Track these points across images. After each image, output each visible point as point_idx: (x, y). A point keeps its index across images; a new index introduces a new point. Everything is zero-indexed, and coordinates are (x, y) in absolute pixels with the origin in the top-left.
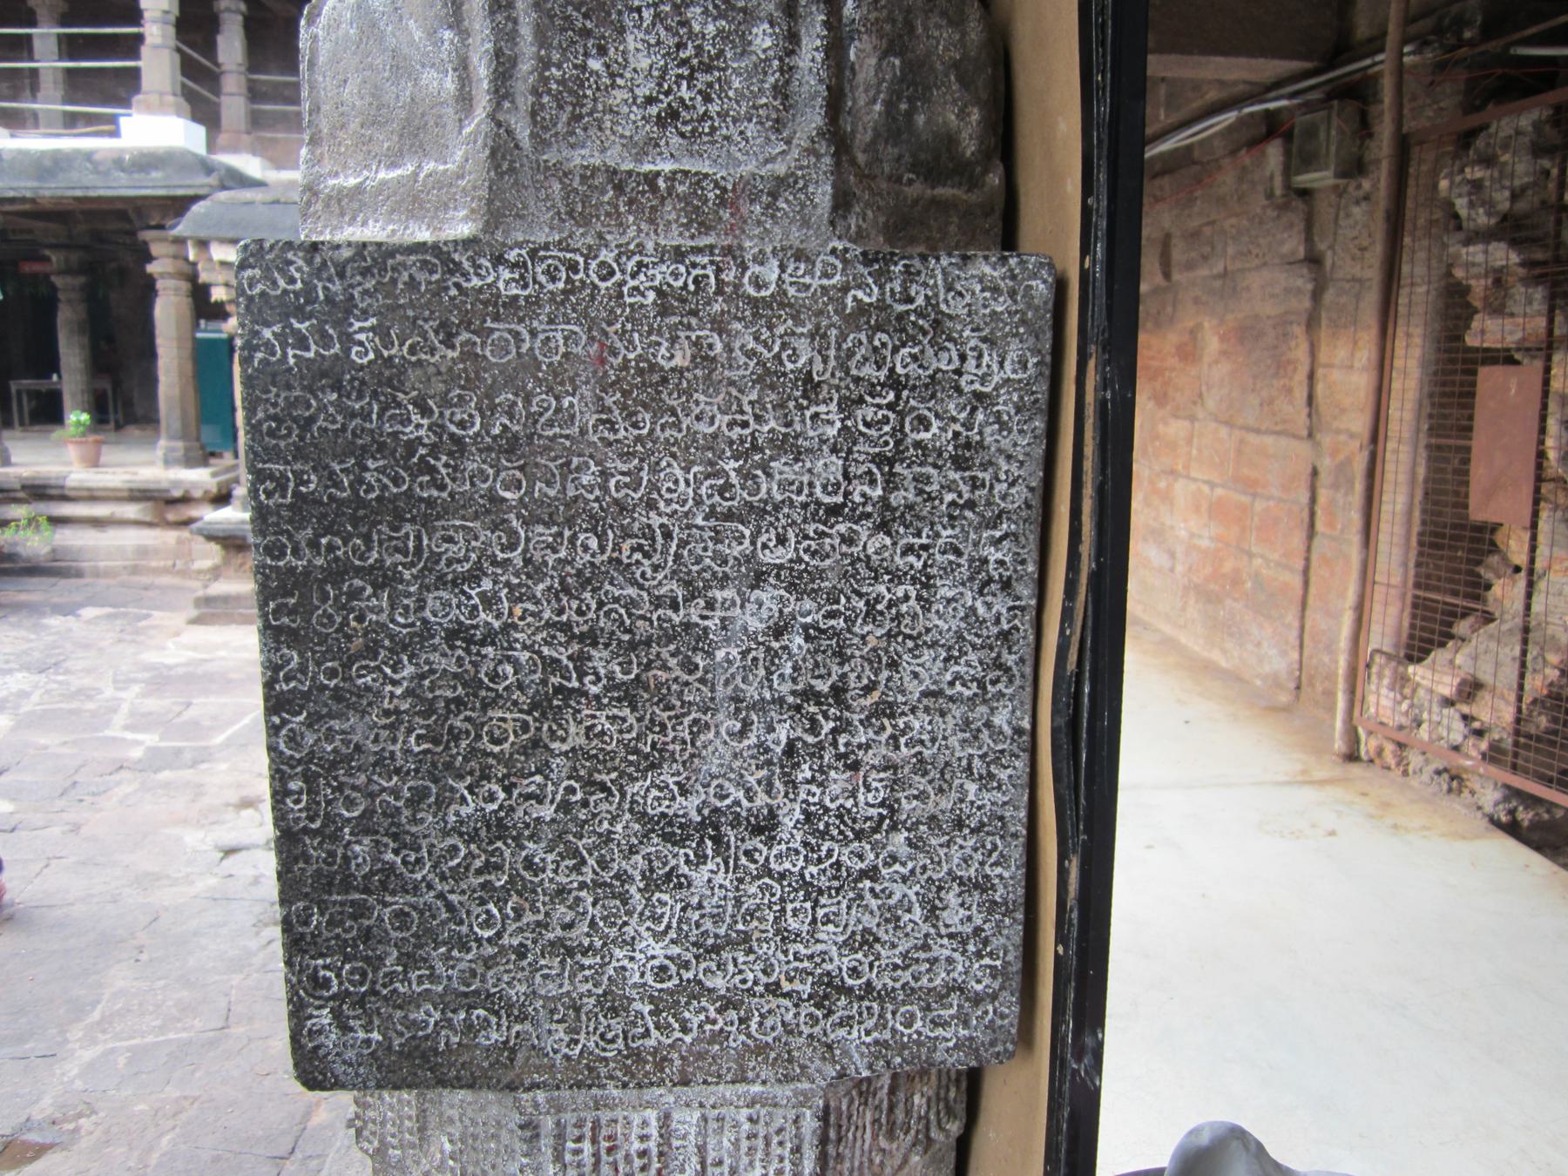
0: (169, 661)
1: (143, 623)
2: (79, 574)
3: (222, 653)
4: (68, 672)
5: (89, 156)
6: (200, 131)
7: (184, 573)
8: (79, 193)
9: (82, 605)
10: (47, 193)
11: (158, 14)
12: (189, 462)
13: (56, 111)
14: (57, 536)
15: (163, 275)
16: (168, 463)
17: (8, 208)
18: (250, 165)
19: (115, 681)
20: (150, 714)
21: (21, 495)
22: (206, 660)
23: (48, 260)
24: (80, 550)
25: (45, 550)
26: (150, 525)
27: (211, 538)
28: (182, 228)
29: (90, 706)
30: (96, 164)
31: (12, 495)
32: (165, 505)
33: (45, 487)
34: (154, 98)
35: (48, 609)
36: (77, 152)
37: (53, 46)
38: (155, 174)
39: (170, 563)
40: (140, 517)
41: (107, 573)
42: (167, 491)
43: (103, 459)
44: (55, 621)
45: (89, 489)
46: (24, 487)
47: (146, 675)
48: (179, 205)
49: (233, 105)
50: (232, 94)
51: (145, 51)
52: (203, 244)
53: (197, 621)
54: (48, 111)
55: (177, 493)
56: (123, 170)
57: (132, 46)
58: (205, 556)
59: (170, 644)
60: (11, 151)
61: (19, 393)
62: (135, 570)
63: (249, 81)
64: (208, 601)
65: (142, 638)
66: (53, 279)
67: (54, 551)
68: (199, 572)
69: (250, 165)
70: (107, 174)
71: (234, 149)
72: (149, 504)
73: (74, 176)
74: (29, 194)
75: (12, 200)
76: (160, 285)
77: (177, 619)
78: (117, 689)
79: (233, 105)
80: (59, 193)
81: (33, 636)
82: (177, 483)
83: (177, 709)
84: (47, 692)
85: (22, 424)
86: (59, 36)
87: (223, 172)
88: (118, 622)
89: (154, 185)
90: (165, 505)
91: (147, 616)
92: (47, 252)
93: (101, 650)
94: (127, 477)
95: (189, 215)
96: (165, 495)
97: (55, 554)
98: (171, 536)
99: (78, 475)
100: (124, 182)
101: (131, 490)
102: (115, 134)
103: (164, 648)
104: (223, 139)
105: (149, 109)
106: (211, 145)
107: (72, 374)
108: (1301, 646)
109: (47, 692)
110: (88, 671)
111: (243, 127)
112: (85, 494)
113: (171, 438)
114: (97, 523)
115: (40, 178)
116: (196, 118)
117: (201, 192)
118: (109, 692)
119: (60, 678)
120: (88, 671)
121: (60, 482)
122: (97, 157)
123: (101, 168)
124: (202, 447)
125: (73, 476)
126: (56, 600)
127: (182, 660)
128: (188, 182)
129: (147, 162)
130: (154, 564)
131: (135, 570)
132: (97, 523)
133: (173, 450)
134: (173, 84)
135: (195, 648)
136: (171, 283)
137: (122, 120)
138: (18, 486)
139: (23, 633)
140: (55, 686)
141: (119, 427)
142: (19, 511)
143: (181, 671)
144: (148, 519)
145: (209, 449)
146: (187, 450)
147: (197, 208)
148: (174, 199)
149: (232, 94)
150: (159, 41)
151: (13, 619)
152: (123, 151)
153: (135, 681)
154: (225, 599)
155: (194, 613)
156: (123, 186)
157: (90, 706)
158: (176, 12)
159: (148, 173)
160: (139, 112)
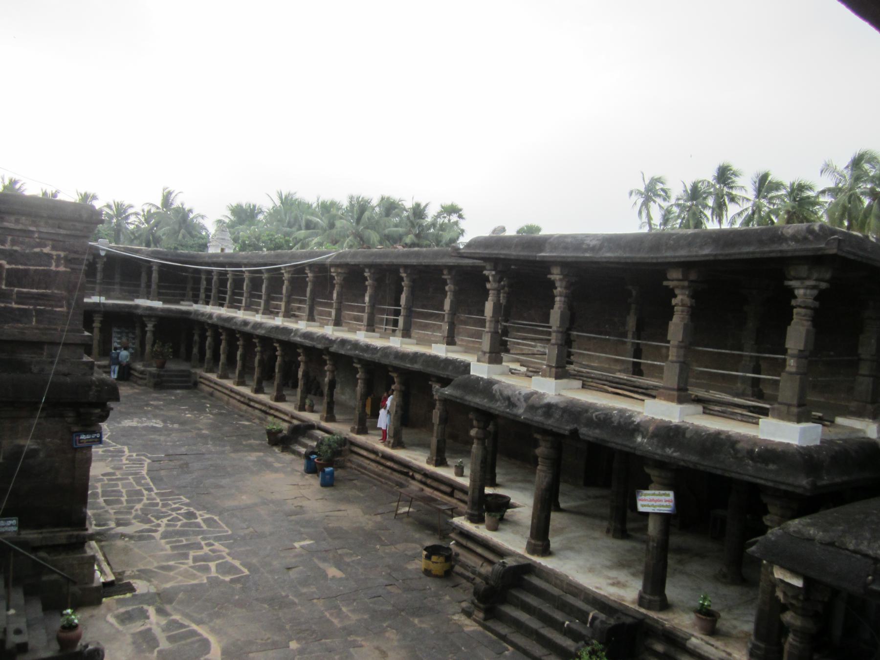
30: (737, 451)
50: (864, 376)
56: (752, 459)
149: (864, 376)
159: (767, 465)
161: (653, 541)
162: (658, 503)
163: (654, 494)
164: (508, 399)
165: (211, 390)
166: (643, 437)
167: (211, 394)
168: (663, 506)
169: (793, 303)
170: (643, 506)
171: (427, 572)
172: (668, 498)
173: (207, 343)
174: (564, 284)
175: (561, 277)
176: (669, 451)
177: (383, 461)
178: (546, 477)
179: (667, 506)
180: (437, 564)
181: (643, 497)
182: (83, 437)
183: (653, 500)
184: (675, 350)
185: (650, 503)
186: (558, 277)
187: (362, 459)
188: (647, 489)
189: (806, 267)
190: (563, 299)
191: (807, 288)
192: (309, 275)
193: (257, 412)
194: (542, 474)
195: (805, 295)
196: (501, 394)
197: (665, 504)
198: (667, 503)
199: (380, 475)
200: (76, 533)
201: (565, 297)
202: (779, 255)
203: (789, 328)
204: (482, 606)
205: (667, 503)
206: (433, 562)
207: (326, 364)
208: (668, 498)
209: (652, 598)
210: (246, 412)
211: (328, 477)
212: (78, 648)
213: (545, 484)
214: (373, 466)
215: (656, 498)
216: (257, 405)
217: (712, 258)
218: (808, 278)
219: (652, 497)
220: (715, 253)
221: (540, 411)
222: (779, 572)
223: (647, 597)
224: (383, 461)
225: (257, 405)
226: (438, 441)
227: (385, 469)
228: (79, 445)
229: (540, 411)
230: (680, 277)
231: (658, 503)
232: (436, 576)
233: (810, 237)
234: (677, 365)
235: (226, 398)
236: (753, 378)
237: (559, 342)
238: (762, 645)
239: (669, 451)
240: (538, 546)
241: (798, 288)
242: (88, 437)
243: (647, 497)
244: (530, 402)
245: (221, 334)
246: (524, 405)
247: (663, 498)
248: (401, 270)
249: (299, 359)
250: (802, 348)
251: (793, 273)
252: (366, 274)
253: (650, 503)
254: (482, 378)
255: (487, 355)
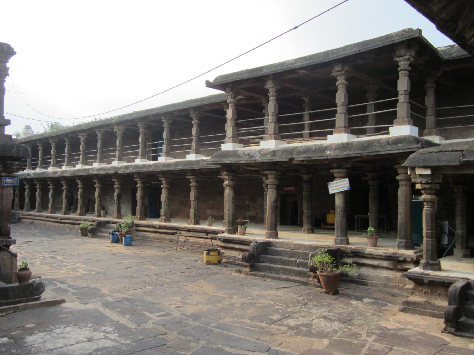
0: (389, 327)
1: (384, 308)
2: (366, 284)
3: (410, 327)
4: (353, 325)
5: (378, 141)
6: (416, 129)
7: (402, 289)
8: (375, 154)
9: (365, 297)
10: (365, 154)
11: (403, 92)
12: (407, 248)
13: (372, 128)
14: (361, 270)
15: (402, 180)
16: (399, 247)
17: (354, 160)
18: (435, 139)
19: (367, 332)
20: (376, 350)
21: (351, 255)
22: (402, 329)
23: (367, 176)
24: (368, 276)
25: (357, 275)
26: (391, 269)
27: (410, 279)
28: (406, 163)
29: (356, 342)
30: (380, 144)
31: (348, 254)
32: (397, 263)
33: (358, 253)
34: (401, 120)
35: (353, 297)
36: (375, 140)
37: (373, 107)
38: (399, 145)
39: (397, 284)
40: (388, 266)
41: (376, 286)
42: (398, 258)
43: (378, 244)
44: (354, 302)
45: (372, 255)
46: (352, 252)
47: (379, 332)
48: (406, 155)
49: (430, 120)
50: (430, 115)
51: (398, 104)
52: (413, 169)
53: (403, 310)
54: (369, 128)
55: (401, 259)
56: (389, 145)
57: (394, 104)
58: (409, 284)
59: (391, 319)
60: (355, 142)
61: (358, 219)
62: (385, 286)
63: (436, 110)
64: (408, 303)
65: (381, 314)
66: (369, 182)
67: (359, 275)
68: (408, 289)
69: (435, 139)
70: (384, 146)
71: (430, 134)
72: (392, 262)
73: (374, 148)
74: (359, 155)
75: (355, 157)
76: (400, 183)
77: (396, 308)
78: (367, 336)
79: (430, 120)
80: (368, 154)
81: (346, 307)
82: (402, 255)
83: (386, 350)
84: (344, 332)
85: (358, 229)
86: (374, 104)
87: (424, 142)
88: (375, 306)
89: (399, 149)
90: (397, 263)
91: (386, 305)
92: (367, 174)
93: (366, 317)
94: (385, 251)
95: (408, 158)
96: (397, 259)
97: (360, 276)
98: (398, 275)
99: (370, 250)
100: (389, 149)
101: (386, 256)
102: (388, 133)
103: (388, 320)
104: (426, 131)
105: (399, 124)
106: (421, 134)
107: (372, 215)
108: (453, 151)
109: (344, 332)
110: (360, 326)
111: (433, 126)
112: (371, 256)
113: (401, 238)
114: (374, 267)
115: (363, 150)
116: (415, 125)
117: (415, 150)
118: (364, 337)
119: (350, 327)
120: (360, 326)
121: (363, 251)
122: (381, 141)
123: (382, 145)
124: (412, 242)
125: (367, 250)
126: (357, 294)
127: (394, 327)
128: (411, 147)
129: (398, 141)
130: (391, 284)
131: (385, 286)
132: (374, 267)
133: (401, 242)
134: (408, 114)
135: (399, 322)
136: (404, 183)
137: (390, 128)
138: (350, 252)
139: (343, 305)
140: (347, 330)
141: (388, 232)
142: (349, 261)
143: (392, 332)
144: (391, 267)
145: (414, 243)
146: (406, 242)
147: (412, 156)
148: (406, 153)
149: (430, 115)
150: (403, 100)
151: (341, 299)
152: (389, 138)
153: (374, 333)
154: (414, 303)
155: (402, 307)
156: (389, 150)
157: (356, 342)
158: (409, 90)
159: (397, 145)
160: (396, 125)
161: (339, 208)
162: (340, 187)
163: (338, 182)
164: (249, 154)
165: (31, 220)
166: (330, 151)
167: (32, 223)
168: (343, 187)
169: (399, 69)
170: (332, 190)
171: (208, 263)
172: (345, 182)
173: (26, 193)
174: (274, 90)
175: (273, 85)
176: (345, 153)
177: (159, 230)
178: (273, 195)
179: (345, 187)
180: (214, 257)
181: (332, 186)
182: (8, 180)
183: (337, 186)
184: (341, 107)
185: (336, 188)
186: (271, 86)
187: (144, 233)
188: (333, 181)
189: (404, 50)
190: (274, 98)
191: (404, 60)
192: (99, 135)
193: (67, 225)
194: (271, 193)
195: (404, 64)
196: (244, 154)
197: (344, 186)
198: (345, 185)
199: (158, 239)
200: (5, 239)
201: (275, 96)
202: (392, 43)
203: (398, 81)
204: (248, 264)
205: (345, 185)
206: (211, 256)
207: (115, 184)
208: (345, 182)
209: (342, 238)
210: (59, 226)
211: (128, 240)
212: (31, 281)
213: (273, 198)
214: (153, 235)
215: (339, 184)
216: (66, 221)
217: (358, 52)
218: (405, 55)
219: (336, 185)
220: (359, 49)
221: (269, 155)
222: (418, 171)
223: (339, 238)
224: (159, 230)
225: (66, 221)
226: (194, 210)
227: (161, 235)
228: (5, 185)
229: (269, 155)
230: (340, 69)
231: (340, 187)
232: (213, 264)
233: (405, 33)
234: (343, 115)
235: (43, 222)
236: (375, 128)
237: (274, 121)
238: (404, 241)
239: (345, 153)
240: (273, 233)
241: (401, 61)
242: (11, 180)
243: (334, 185)
244: (262, 153)
245: (36, 185)
246: (259, 155)
247: (343, 183)
248: (163, 118)
249: (95, 186)
250: (406, 89)
251: (397, 54)
252: (139, 126)
253: (336, 188)
254: (230, 151)
255: (231, 138)
